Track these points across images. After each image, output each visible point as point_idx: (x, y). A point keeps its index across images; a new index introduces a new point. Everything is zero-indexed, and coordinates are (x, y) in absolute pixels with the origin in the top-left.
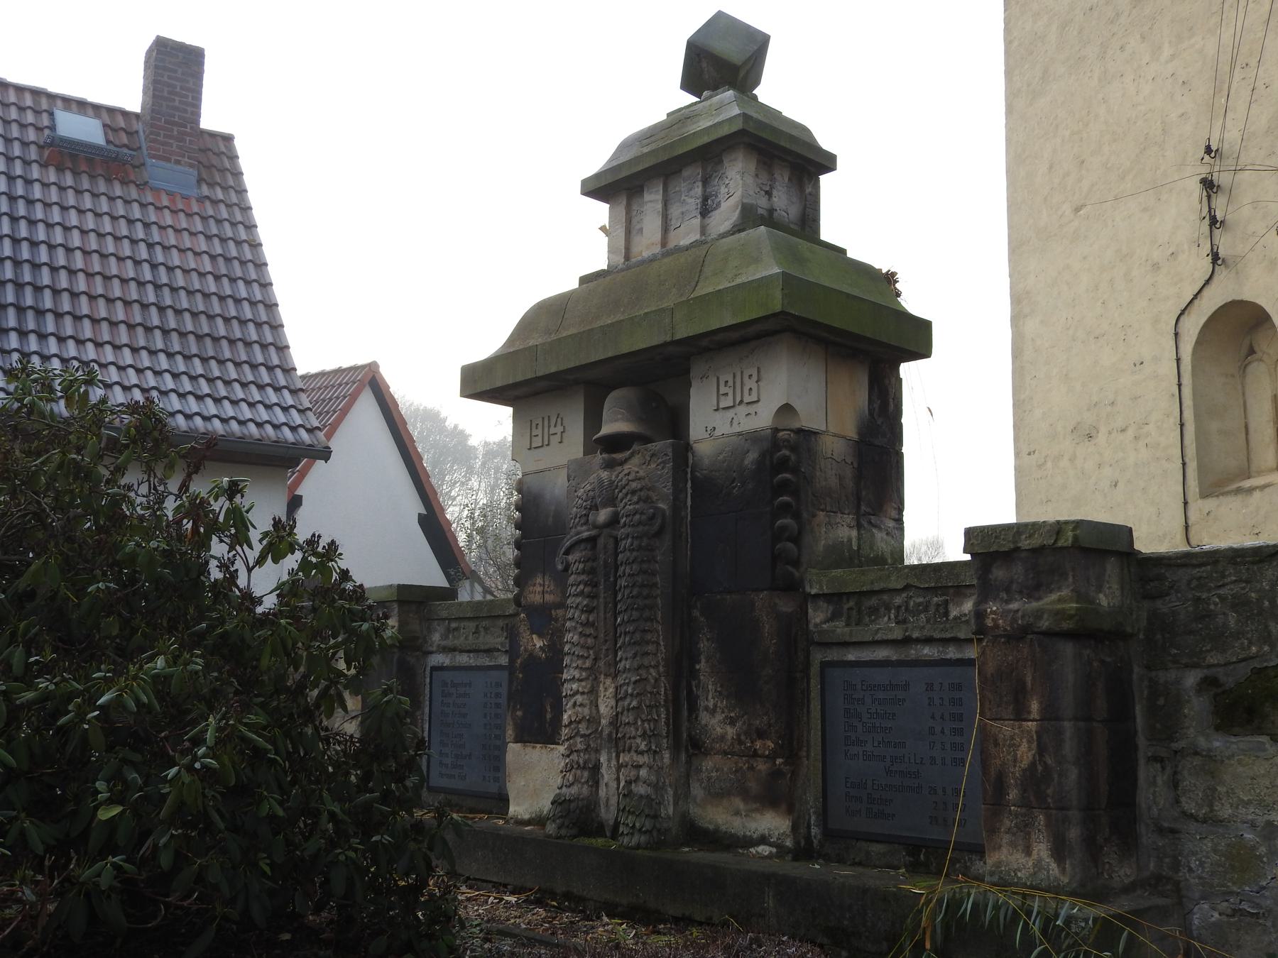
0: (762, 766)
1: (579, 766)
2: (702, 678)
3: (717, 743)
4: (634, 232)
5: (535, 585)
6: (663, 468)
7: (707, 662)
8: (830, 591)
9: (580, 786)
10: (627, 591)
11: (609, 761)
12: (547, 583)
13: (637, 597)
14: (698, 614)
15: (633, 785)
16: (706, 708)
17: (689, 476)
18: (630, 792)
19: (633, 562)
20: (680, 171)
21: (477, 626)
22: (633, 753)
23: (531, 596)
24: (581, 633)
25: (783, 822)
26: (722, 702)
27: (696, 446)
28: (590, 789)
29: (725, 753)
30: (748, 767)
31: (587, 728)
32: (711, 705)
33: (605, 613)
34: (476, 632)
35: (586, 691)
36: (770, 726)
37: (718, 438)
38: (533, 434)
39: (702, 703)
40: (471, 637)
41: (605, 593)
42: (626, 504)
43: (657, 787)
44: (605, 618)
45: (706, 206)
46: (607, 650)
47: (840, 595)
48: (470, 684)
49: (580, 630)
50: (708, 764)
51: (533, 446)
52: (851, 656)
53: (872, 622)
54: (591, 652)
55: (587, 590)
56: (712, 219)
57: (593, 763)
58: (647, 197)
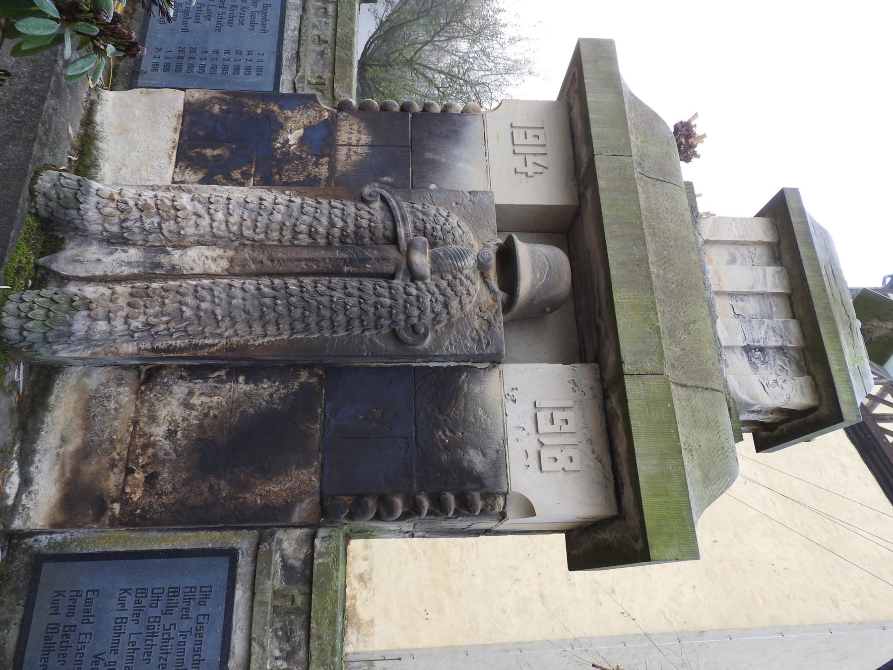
0: (113, 480)
1: (124, 221)
2: (228, 386)
3: (149, 410)
4: (732, 249)
5: (359, 132)
6: (473, 339)
7: (245, 394)
8: (315, 567)
9: (100, 221)
10: (325, 300)
11: (129, 264)
12: (360, 150)
13: (318, 314)
14: (302, 380)
15: (86, 313)
16: (191, 393)
17: (463, 364)
18: (76, 309)
19: (361, 308)
20: (794, 317)
21: (326, 42)
22: (127, 310)
23: (348, 126)
24: (284, 224)
25: (42, 516)
26: (196, 417)
27: (496, 372)
28: (99, 233)
29: (135, 423)
30: (114, 460)
31: (170, 231)
32: (196, 401)
33: (308, 260)
34: (321, 41)
35: (215, 230)
36: (160, 495)
37: (503, 406)
38: (528, 157)
39: (198, 386)
40: (316, 32)
41: (330, 259)
42: (433, 294)
43: (87, 340)
44: (299, 260)
45: (755, 349)
46: (262, 262)
47: (309, 582)
48: (264, 31)
49: (287, 224)
50: (125, 395)
51: (515, 131)
52: (240, 595)
53: (275, 632)
54: (262, 236)
55: (336, 232)
56: (740, 358)
57: (130, 237)
58: (771, 270)
